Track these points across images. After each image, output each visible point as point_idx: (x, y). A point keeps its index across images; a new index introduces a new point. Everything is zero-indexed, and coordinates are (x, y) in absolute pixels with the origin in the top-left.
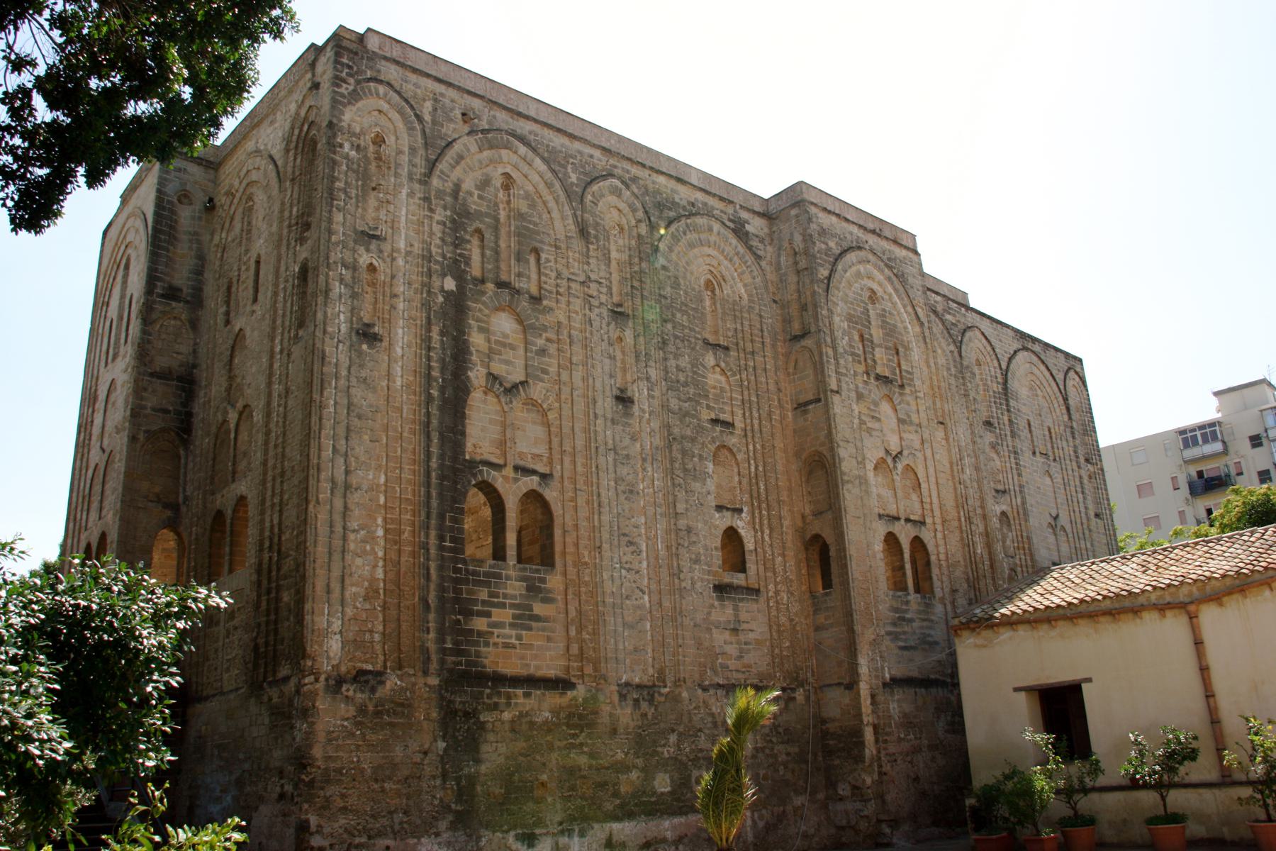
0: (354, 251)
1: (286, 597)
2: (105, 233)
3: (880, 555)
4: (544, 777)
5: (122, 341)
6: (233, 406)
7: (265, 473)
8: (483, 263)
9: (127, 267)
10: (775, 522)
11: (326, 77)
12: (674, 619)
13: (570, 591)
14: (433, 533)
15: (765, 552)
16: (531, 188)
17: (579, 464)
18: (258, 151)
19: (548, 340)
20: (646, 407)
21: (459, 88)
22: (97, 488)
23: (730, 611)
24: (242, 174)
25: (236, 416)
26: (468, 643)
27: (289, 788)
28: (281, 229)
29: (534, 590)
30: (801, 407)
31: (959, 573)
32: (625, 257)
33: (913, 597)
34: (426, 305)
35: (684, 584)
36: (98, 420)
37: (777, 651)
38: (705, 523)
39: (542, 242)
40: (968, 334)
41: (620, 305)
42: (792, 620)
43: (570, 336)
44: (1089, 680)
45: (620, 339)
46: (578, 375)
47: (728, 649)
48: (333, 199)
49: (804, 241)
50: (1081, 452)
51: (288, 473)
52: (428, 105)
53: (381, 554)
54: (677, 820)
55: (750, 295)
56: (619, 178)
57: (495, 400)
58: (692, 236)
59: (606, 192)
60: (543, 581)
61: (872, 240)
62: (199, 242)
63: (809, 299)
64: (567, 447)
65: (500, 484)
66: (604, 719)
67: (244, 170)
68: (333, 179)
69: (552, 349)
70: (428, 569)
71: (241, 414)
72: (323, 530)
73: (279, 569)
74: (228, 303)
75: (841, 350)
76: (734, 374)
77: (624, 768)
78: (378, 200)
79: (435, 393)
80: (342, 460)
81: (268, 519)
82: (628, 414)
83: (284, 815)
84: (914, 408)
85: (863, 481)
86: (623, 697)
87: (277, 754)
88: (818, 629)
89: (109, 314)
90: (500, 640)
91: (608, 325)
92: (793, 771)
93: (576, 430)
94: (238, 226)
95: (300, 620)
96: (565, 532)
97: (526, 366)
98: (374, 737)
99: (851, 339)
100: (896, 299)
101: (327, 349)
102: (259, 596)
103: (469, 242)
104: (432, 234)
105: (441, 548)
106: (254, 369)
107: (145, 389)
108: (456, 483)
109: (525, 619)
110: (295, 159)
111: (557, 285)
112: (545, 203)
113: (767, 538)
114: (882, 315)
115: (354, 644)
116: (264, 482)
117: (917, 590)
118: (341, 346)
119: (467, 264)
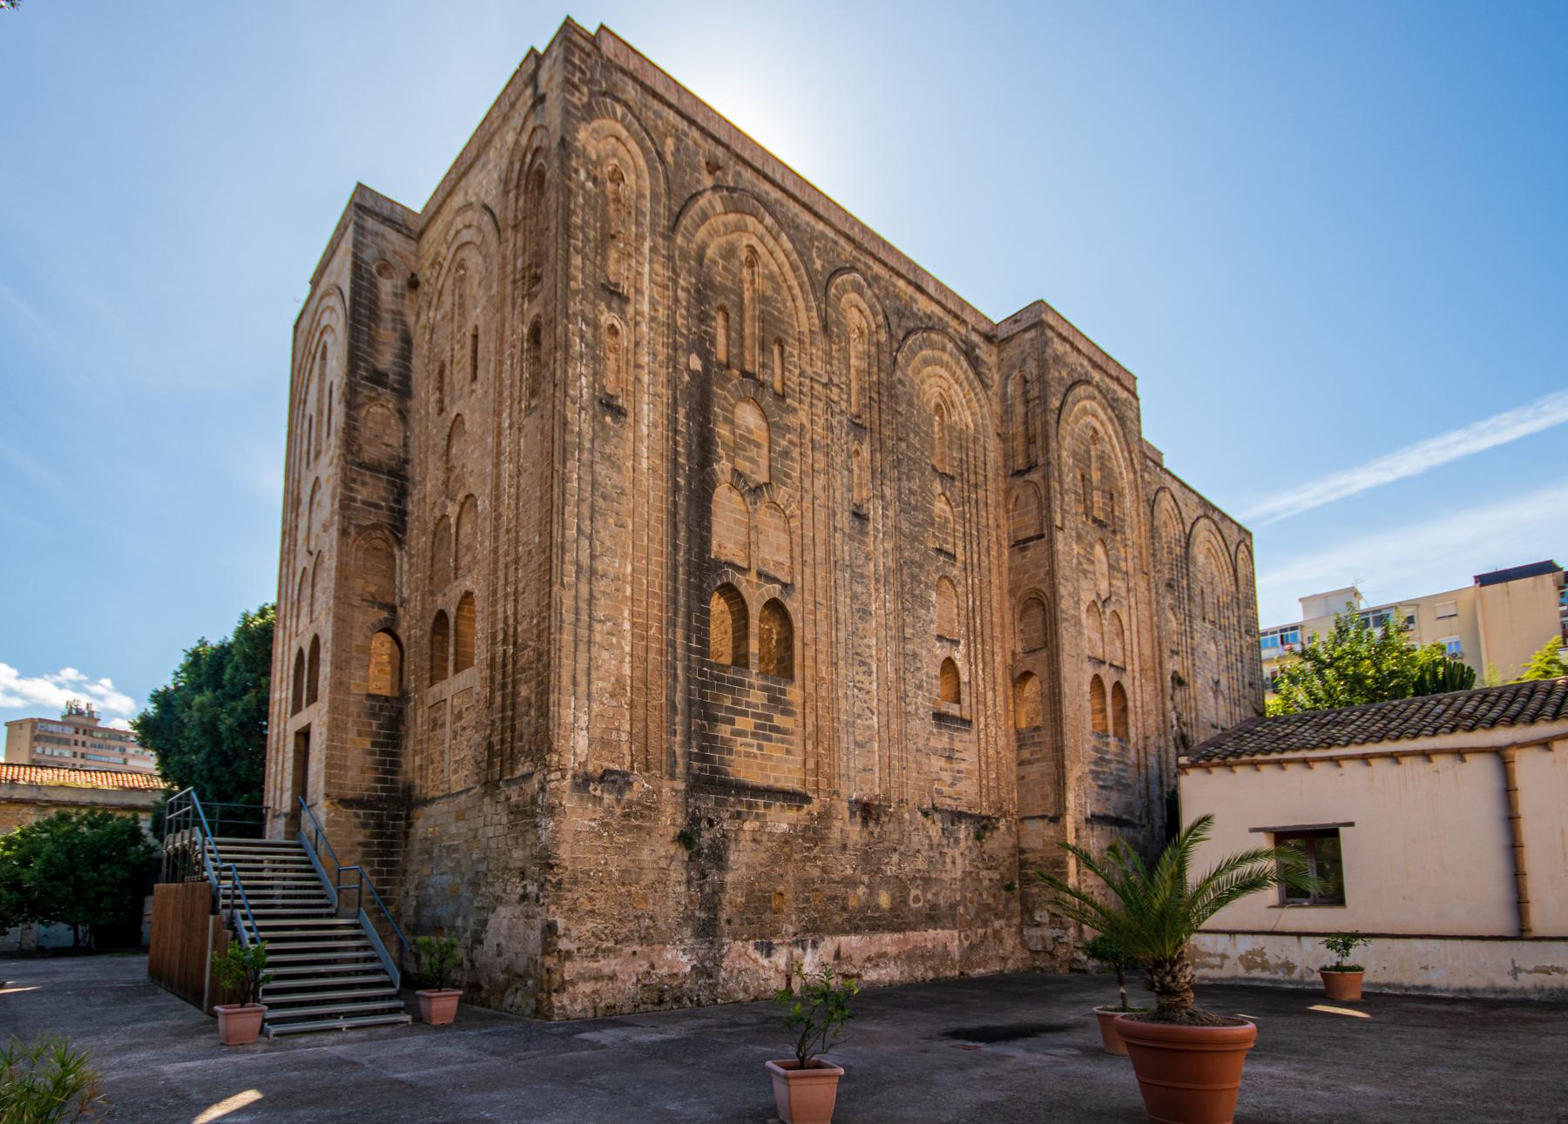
0: (595, 306)
1: (524, 691)
2: (296, 327)
3: (1088, 696)
4: (781, 888)
5: (324, 435)
6: (453, 500)
7: (496, 561)
8: (728, 345)
9: (324, 357)
11: (554, 84)
12: (899, 742)
13: (808, 706)
14: (680, 632)
16: (775, 268)
18: (469, 206)
19: (791, 442)
21: (702, 130)
22: (307, 592)
23: (945, 739)
25: (457, 508)
26: (712, 748)
27: (532, 889)
29: (777, 702)
30: (1020, 545)
31: (1151, 721)
32: (864, 365)
33: (1112, 740)
34: (672, 382)
36: (303, 524)
39: (785, 332)
40: (1161, 494)
41: (859, 417)
42: (998, 753)
43: (812, 441)
44: (1351, 824)
45: (857, 453)
46: (820, 481)
47: (944, 775)
51: (524, 560)
52: (670, 141)
53: (627, 649)
54: (896, 936)
55: (976, 425)
56: (863, 275)
58: (927, 352)
59: (848, 287)
60: (783, 692)
61: (1096, 376)
62: (404, 323)
65: (744, 589)
66: (835, 834)
67: (452, 232)
68: (569, 213)
69: (796, 453)
71: (462, 505)
72: (569, 617)
73: (515, 662)
74: (440, 389)
78: (619, 251)
79: (681, 481)
80: (587, 543)
81: (500, 609)
83: (527, 917)
85: (1078, 623)
86: (853, 814)
87: (517, 854)
88: (1021, 763)
90: (742, 749)
92: (994, 896)
94: (448, 300)
95: (544, 712)
96: (804, 644)
102: (492, 692)
104: (677, 300)
105: (689, 649)
106: (476, 454)
107: (354, 481)
108: (702, 581)
109: (767, 730)
110: (517, 200)
111: (801, 384)
112: (790, 288)
114: (1102, 457)
115: (602, 743)
117: (1115, 734)
119: (713, 343)
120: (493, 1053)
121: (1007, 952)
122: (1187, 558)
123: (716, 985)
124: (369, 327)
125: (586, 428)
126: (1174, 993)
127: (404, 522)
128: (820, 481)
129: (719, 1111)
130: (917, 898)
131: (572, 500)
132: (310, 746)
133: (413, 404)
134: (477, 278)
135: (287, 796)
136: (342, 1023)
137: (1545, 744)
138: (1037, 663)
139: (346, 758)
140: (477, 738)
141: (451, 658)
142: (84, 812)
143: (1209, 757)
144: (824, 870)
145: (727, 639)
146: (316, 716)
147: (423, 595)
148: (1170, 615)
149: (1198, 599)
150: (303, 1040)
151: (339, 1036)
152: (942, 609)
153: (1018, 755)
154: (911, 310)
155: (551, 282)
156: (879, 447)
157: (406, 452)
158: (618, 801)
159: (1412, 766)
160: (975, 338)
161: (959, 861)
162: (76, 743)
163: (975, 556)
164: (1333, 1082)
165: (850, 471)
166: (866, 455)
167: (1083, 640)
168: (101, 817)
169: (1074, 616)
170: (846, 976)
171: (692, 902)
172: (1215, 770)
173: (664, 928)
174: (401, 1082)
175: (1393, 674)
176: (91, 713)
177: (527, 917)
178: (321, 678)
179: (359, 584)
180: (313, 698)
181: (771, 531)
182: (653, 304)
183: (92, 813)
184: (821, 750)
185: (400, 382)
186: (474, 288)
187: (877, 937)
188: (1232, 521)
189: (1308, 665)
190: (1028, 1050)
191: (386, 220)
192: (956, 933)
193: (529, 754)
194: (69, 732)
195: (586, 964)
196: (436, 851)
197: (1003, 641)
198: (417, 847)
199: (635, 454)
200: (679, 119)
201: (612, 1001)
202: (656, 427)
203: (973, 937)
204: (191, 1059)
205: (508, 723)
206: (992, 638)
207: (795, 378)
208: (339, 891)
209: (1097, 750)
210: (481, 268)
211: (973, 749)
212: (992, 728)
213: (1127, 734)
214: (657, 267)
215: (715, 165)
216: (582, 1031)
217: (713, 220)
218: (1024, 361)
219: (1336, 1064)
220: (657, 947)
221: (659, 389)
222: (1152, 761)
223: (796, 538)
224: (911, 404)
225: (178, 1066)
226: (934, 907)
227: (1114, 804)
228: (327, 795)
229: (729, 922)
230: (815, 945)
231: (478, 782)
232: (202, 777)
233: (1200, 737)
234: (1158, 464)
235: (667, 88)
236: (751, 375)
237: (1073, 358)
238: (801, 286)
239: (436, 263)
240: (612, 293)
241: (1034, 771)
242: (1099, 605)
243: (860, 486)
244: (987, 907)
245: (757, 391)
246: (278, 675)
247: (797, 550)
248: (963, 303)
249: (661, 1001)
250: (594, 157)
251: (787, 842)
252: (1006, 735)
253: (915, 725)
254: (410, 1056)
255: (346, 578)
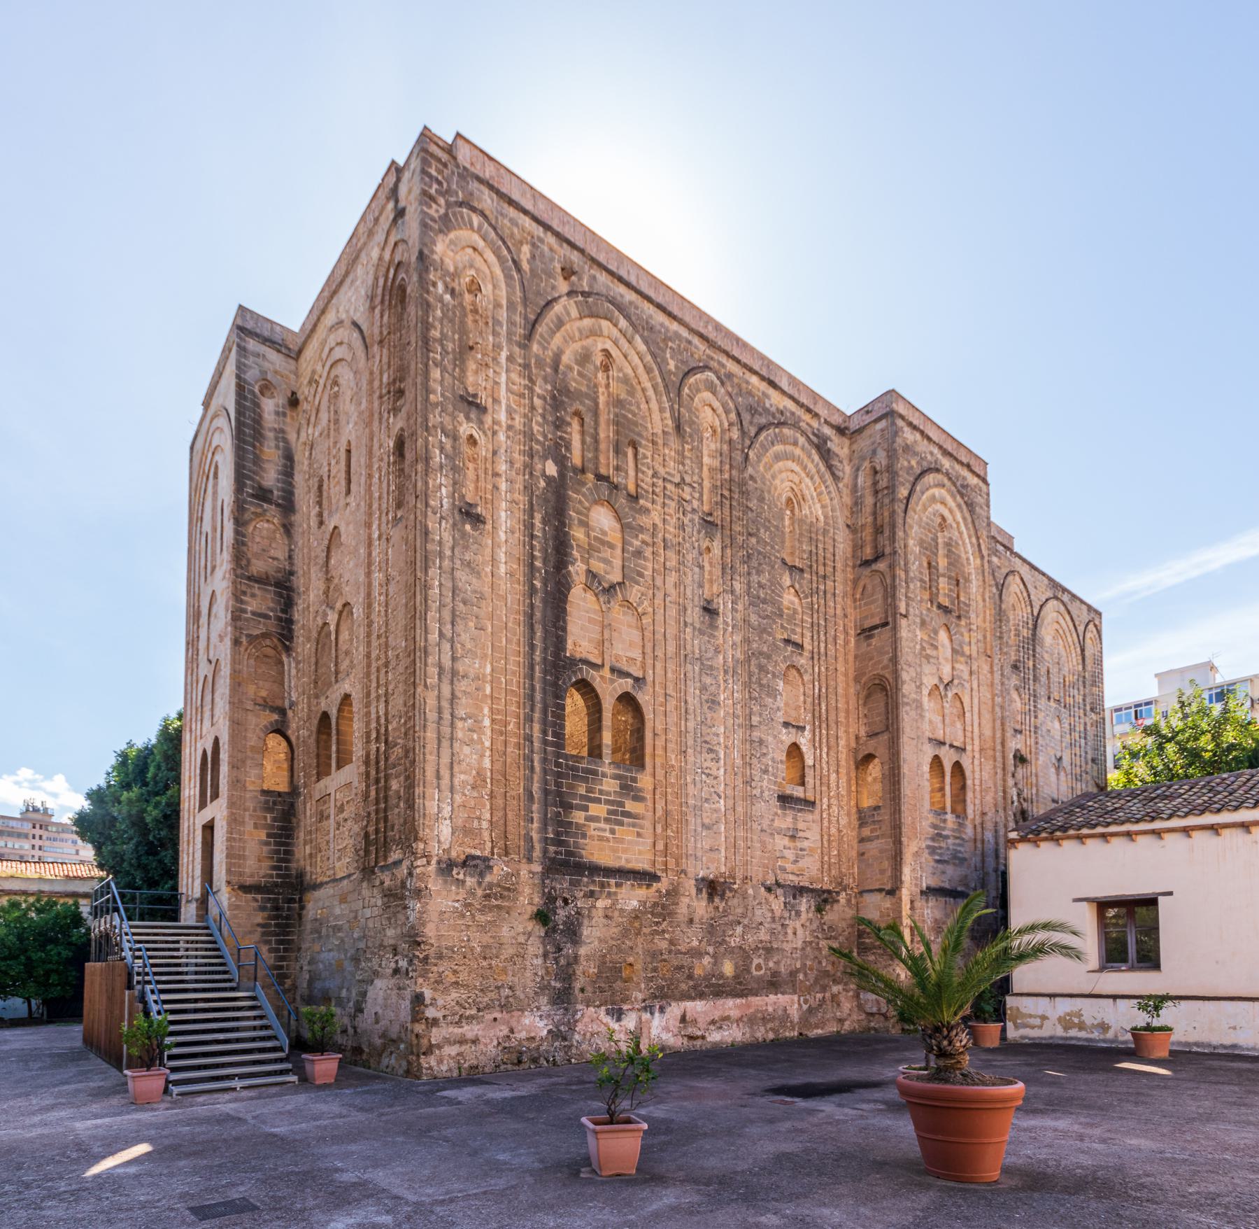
0: (454, 418)
1: (395, 785)
2: (192, 448)
3: (927, 776)
4: (631, 960)
6: (332, 608)
7: (369, 666)
8: (583, 450)
10: (832, 741)
11: (412, 197)
13: (658, 792)
15: (822, 768)
16: (629, 371)
17: (669, 671)
18: (341, 322)
19: (643, 542)
20: (729, 620)
21: (557, 235)
22: (208, 698)
23: (789, 819)
24: (324, 356)
25: (336, 616)
26: (567, 834)
27: (403, 964)
28: (371, 402)
29: (628, 788)
30: (866, 633)
31: (989, 798)
32: (716, 463)
33: (950, 817)
34: (528, 489)
35: (754, 792)
37: (826, 858)
38: (775, 737)
39: (640, 435)
40: (1010, 578)
41: (710, 514)
42: (840, 831)
43: (664, 540)
44: (1170, 893)
45: (708, 549)
46: (672, 578)
48: (428, 350)
49: (889, 457)
50: (1088, 700)
51: (393, 663)
52: (526, 249)
53: (487, 744)
54: (738, 1001)
55: (826, 517)
56: (716, 373)
57: (594, 599)
58: (779, 448)
59: (702, 386)
60: (634, 780)
61: (946, 463)
62: (286, 441)
63: (887, 520)
64: (660, 653)
65: (597, 684)
66: (682, 910)
68: (427, 327)
69: (648, 552)
70: (532, 761)
71: (341, 613)
72: (432, 716)
73: (387, 759)
74: (320, 503)
75: (912, 574)
76: (806, 597)
77: (697, 953)
78: (476, 362)
79: (538, 584)
80: (448, 646)
81: (373, 710)
82: (713, 626)
83: (399, 989)
84: (967, 640)
85: (919, 706)
86: (699, 891)
87: (390, 932)
88: (862, 840)
89: (204, 530)
91: (699, 532)
92: (833, 963)
93: (668, 636)
94: (324, 416)
95: (411, 805)
96: (655, 734)
97: (623, 567)
98: (483, 918)
99: (921, 565)
100: (963, 528)
101: (430, 525)
102: (368, 786)
103: (569, 424)
104: (533, 408)
105: (545, 742)
106: (352, 564)
107: (244, 593)
108: (558, 679)
109: (618, 815)
110: (382, 316)
111: (654, 485)
112: (643, 390)
113: (824, 756)
115: (465, 831)
116: (368, 674)
117: (953, 811)
118: (444, 522)
119: (568, 449)
120: (361, 1109)
121: (846, 1012)
122: (1034, 638)
123: (570, 1047)
124: (254, 447)
125: (447, 537)
126: (951, 1056)
127: (291, 631)
128: (672, 578)
129: (541, 1161)
130: (759, 967)
131: (434, 606)
132: (216, 840)
133: (296, 518)
134: (349, 393)
135: (198, 882)
136: (237, 1083)
137: (1245, 826)
138: (879, 746)
139: (244, 849)
140: (356, 828)
141: (334, 756)
142: (31, 899)
143: (1037, 832)
144: (672, 942)
145: (581, 728)
146: (218, 811)
147: (309, 698)
148: (1015, 696)
149: (1043, 680)
150: (201, 1099)
151: (234, 1094)
152: (789, 697)
153: (859, 833)
154: (764, 406)
155: (412, 395)
156: (730, 542)
157: (291, 564)
158: (480, 883)
159: (1236, 836)
160: (827, 431)
161: (800, 932)
162: (34, 837)
163: (822, 645)
164: (1112, 1136)
165: (701, 567)
166: (717, 550)
167: (924, 722)
168: (47, 903)
169: (915, 700)
170: (691, 1038)
171: (548, 973)
172: (1043, 845)
173: (522, 996)
174: (275, 1136)
175: (1232, 747)
176: (46, 810)
177: (399, 989)
178: (221, 777)
179: (251, 690)
180: (215, 795)
181: (624, 628)
182: (510, 412)
183: (38, 900)
184: (670, 833)
185: (284, 498)
186: (347, 407)
187: (720, 1002)
188: (1082, 602)
189: (1150, 740)
190: (840, 1105)
191: (267, 341)
192: (796, 998)
193: (398, 842)
194: (27, 827)
195: (451, 1029)
196: (324, 931)
197: (847, 725)
198: (309, 927)
199: (493, 559)
200: (534, 225)
201: (476, 1063)
202: (513, 533)
203: (811, 1001)
204: (102, 1117)
205: (382, 815)
206: (837, 723)
207: (648, 480)
208: (239, 967)
209: (934, 826)
210: (352, 384)
211: (816, 828)
212: (835, 808)
213: (965, 810)
214: (514, 376)
215: (573, 271)
216: (445, 1089)
217: (568, 326)
218: (874, 452)
219: (1121, 1118)
220: (516, 1014)
221: (516, 495)
222: (989, 835)
223: (648, 634)
224: (761, 499)
225: (89, 1123)
226: (775, 974)
227: (950, 876)
228: (228, 882)
229: (582, 990)
230: (662, 1010)
231: (358, 868)
232: (131, 865)
233: (1039, 810)
234: (1008, 548)
235: (523, 194)
236: (605, 479)
237: (923, 446)
238: (655, 387)
239: (312, 381)
240: (470, 403)
241: (873, 847)
242: (942, 689)
243: (711, 581)
244: (826, 974)
245: (610, 494)
246: (187, 774)
247: (649, 646)
248: (815, 396)
249: (520, 1062)
250: (452, 269)
251: (637, 917)
252: (849, 814)
253: (760, 807)
254: (289, 1112)
255: (239, 684)
